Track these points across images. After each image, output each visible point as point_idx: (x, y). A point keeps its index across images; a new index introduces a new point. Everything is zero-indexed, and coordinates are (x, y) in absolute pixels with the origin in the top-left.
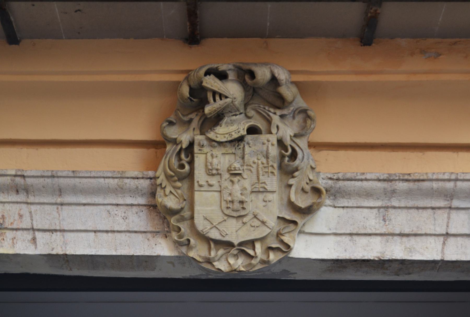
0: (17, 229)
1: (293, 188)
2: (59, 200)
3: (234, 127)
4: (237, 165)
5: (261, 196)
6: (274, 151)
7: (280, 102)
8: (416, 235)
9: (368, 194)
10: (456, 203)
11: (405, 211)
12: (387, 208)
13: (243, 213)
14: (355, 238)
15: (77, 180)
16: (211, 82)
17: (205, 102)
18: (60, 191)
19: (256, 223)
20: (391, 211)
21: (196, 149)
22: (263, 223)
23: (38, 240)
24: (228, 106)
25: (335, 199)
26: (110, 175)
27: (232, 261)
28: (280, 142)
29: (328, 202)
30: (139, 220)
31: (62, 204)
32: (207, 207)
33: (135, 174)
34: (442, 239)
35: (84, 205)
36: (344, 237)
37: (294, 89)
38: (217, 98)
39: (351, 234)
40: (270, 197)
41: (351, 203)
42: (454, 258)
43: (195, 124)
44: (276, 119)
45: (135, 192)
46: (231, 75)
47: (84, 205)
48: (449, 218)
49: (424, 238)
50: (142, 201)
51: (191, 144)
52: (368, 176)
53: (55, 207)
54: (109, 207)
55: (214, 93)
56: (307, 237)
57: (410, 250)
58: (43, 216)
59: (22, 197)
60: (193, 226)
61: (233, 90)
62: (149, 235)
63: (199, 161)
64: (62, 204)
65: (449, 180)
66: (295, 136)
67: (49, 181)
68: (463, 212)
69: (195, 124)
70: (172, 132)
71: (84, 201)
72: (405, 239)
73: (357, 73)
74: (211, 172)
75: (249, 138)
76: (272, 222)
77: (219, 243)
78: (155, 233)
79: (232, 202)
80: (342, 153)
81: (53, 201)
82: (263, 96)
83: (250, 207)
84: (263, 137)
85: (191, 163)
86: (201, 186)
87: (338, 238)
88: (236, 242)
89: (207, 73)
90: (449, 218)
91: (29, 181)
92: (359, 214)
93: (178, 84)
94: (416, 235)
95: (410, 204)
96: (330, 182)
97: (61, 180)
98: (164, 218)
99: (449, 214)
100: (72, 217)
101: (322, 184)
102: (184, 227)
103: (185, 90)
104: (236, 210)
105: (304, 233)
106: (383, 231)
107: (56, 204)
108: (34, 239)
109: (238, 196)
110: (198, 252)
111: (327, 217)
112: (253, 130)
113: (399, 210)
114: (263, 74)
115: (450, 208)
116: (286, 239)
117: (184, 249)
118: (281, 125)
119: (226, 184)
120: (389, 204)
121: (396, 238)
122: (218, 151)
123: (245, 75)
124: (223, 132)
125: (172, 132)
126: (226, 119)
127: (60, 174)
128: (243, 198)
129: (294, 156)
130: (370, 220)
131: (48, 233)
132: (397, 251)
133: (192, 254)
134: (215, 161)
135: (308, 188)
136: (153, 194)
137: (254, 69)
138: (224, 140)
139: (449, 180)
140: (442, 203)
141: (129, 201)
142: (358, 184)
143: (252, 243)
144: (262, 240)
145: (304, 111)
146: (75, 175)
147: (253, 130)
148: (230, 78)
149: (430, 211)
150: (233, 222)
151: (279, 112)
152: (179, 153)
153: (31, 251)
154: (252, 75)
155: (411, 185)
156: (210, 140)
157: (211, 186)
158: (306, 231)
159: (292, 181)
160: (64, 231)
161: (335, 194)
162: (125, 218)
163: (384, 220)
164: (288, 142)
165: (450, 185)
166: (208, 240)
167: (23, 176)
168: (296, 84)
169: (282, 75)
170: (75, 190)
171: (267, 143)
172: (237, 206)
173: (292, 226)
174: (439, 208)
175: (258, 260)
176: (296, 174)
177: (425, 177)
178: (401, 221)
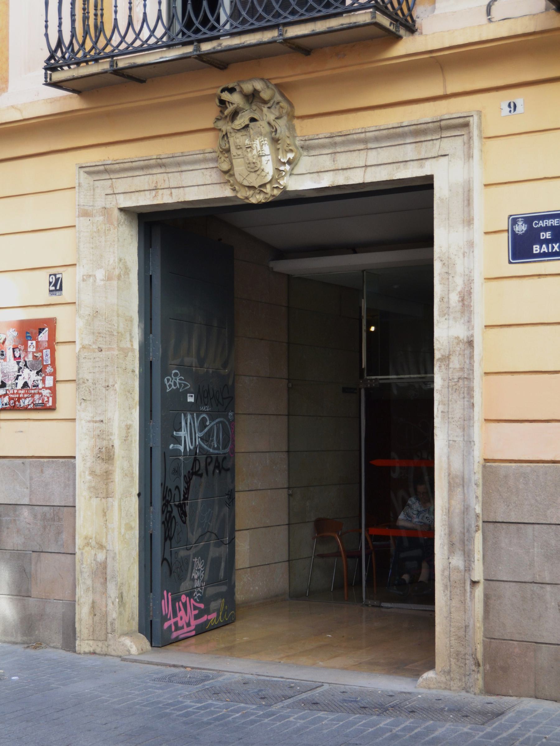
0: (163, 189)
1: (280, 151)
2: (180, 169)
3: (242, 120)
8: (350, 168)
9: (323, 146)
11: (344, 154)
12: (335, 153)
13: (256, 169)
14: (320, 174)
15: (184, 157)
16: (226, 96)
21: (228, 134)
23: (173, 194)
25: (308, 151)
26: (198, 152)
31: (182, 172)
34: (364, 169)
35: (192, 170)
36: (314, 174)
38: (231, 105)
39: (318, 172)
42: (369, 181)
47: (192, 170)
48: (367, 155)
49: (354, 170)
52: (320, 136)
53: (179, 173)
54: (203, 170)
55: (229, 102)
56: (296, 177)
57: (347, 178)
58: (174, 179)
59: (162, 170)
62: (222, 185)
63: (231, 140)
65: (362, 133)
66: (277, 118)
67: (172, 159)
68: (374, 150)
71: (191, 169)
72: (345, 171)
73: (305, 74)
74: (239, 148)
75: (252, 125)
79: (249, 163)
80: (315, 120)
81: (177, 170)
86: (234, 156)
87: (312, 175)
88: (257, 186)
89: (223, 91)
90: (367, 155)
91: (164, 161)
92: (322, 159)
94: (350, 168)
95: (419, 126)
96: (302, 142)
97: (177, 158)
99: (367, 152)
105: (293, 174)
107: (179, 172)
108: (171, 193)
110: (242, 194)
113: (341, 154)
115: (367, 149)
118: (267, 114)
120: (335, 151)
121: (340, 171)
126: (240, 115)
127: (176, 155)
128: (254, 161)
130: (325, 161)
131: (177, 189)
132: (341, 180)
134: (238, 141)
138: (239, 128)
139: (362, 133)
140: (362, 146)
142: (316, 141)
147: (253, 120)
148: (237, 90)
149: (357, 152)
155: (343, 138)
157: (239, 155)
158: (295, 173)
159: (279, 146)
160: (183, 187)
162: (211, 176)
163: (334, 161)
164: (273, 123)
165: (363, 135)
167: (161, 159)
171: (262, 125)
172: (252, 165)
174: (362, 150)
175: (270, 195)
176: (279, 142)
177: (349, 133)
178: (343, 160)
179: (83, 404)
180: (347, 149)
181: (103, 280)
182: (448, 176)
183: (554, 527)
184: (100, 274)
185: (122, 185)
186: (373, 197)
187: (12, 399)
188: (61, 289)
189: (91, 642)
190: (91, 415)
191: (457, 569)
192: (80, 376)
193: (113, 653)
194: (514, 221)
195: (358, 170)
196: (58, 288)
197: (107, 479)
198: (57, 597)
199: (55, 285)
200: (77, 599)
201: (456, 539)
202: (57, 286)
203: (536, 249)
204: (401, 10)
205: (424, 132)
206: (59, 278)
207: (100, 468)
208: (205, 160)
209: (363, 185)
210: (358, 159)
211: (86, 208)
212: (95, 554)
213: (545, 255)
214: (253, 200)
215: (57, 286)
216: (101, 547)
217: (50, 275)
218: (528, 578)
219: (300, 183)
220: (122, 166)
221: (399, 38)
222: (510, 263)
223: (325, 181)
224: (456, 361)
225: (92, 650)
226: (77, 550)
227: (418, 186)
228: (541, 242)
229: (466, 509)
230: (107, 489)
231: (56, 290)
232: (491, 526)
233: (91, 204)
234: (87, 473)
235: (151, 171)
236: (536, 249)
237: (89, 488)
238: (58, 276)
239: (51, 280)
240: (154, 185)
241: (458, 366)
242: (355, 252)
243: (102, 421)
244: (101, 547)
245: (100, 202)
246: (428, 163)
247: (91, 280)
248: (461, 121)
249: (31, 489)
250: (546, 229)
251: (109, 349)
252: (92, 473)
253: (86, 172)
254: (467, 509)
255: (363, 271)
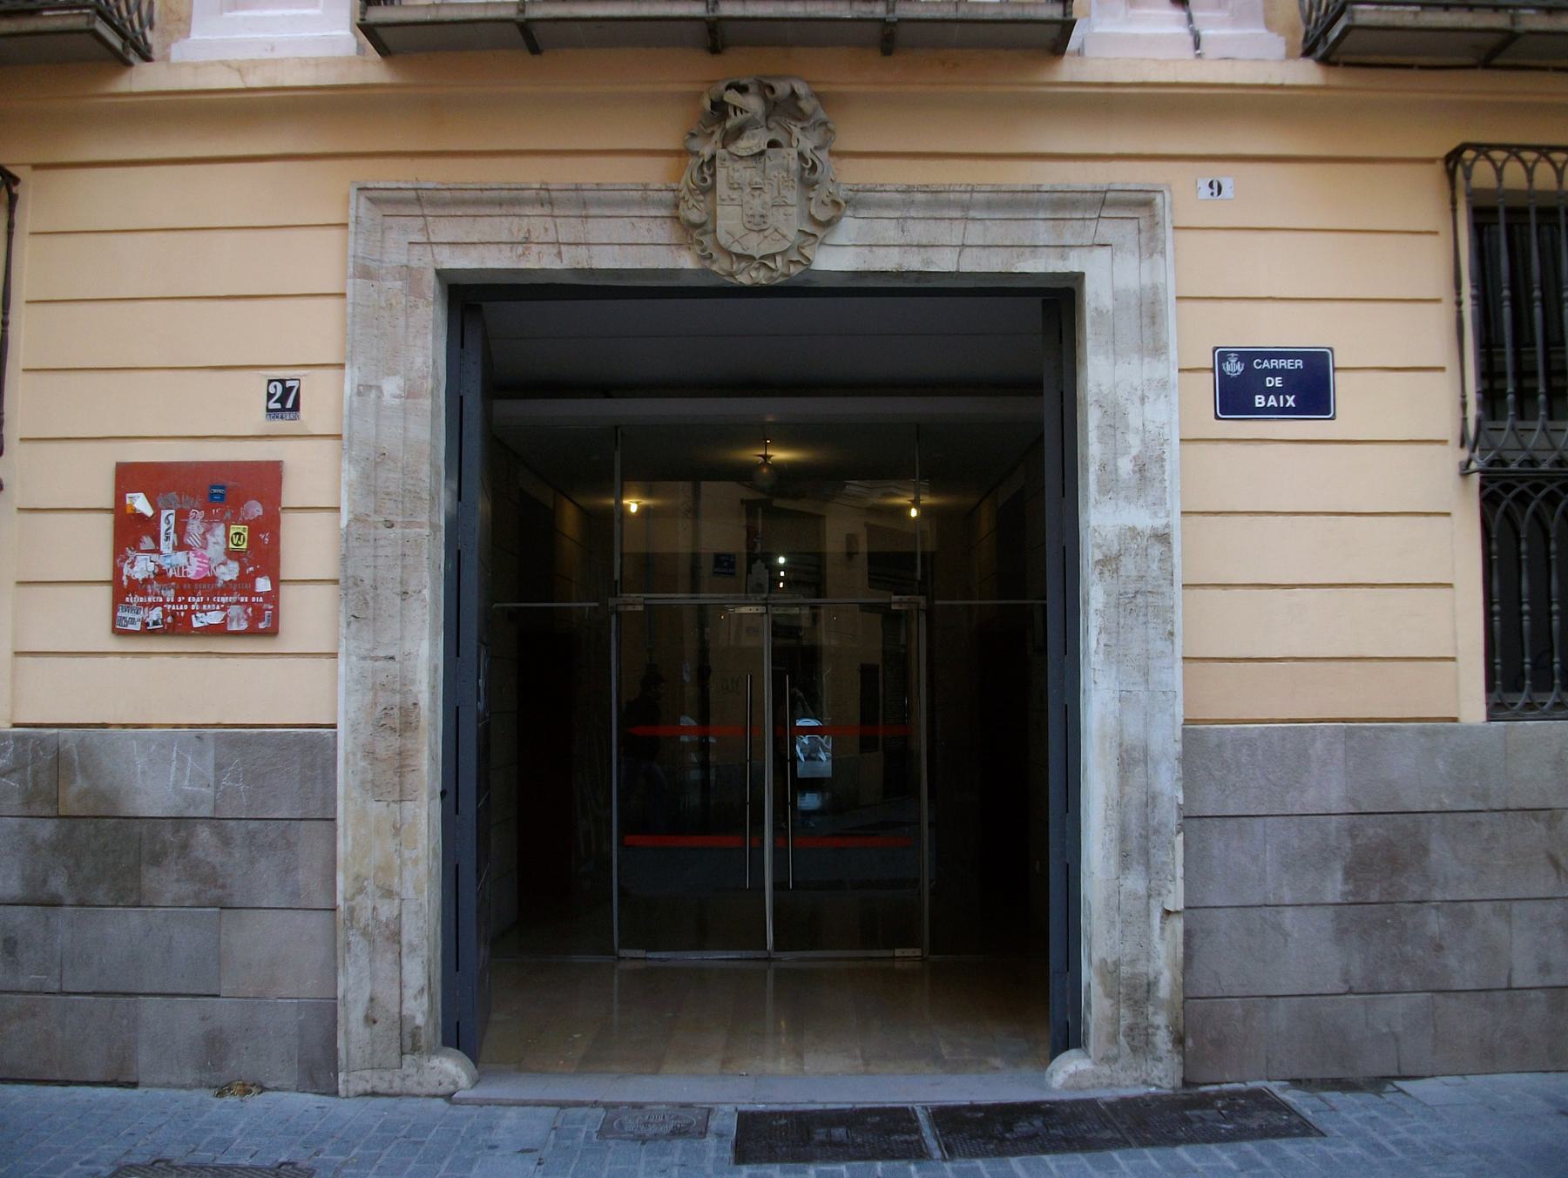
4: (758, 180)
5: (782, 210)
6: (794, 165)
7: (800, 116)
9: (888, 205)
10: (972, 214)
16: (732, 97)
17: (725, 116)
18: (585, 204)
19: (777, 236)
20: (910, 222)
22: (784, 237)
24: (748, 121)
27: (754, 274)
28: (801, 155)
29: (849, 213)
30: (663, 232)
31: (587, 217)
32: (729, 222)
33: (657, 186)
37: (815, 102)
40: (790, 210)
41: (871, 213)
42: (969, 270)
43: (717, 136)
44: (796, 131)
45: (659, 203)
46: (753, 89)
50: (664, 212)
51: (713, 157)
55: (735, 108)
57: (928, 262)
59: (546, 210)
60: (716, 241)
61: (753, 104)
63: (721, 174)
64: (587, 217)
69: (717, 136)
70: (695, 145)
75: (770, 151)
76: (792, 235)
77: (740, 257)
78: (679, 245)
82: (784, 109)
83: (770, 220)
84: (784, 151)
85: (713, 175)
89: (729, 87)
93: (700, 95)
98: (692, 232)
100: (600, 230)
101: (842, 195)
102: (707, 240)
103: (707, 104)
104: (758, 224)
106: (902, 242)
108: (560, 253)
109: (760, 210)
110: (721, 265)
111: (849, 227)
112: (773, 144)
114: (782, 88)
116: (807, 252)
117: (707, 263)
119: (747, 198)
122: (739, 165)
123: (766, 89)
124: (746, 145)
125: (695, 145)
129: (814, 168)
130: (888, 230)
132: (914, 262)
133: (715, 268)
134: (737, 175)
135: (827, 200)
136: (677, 206)
137: (774, 84)
140: (958, 214)
141: (653, 212)
143: (773, 256)
144: (783, 253)
145: (824, 123)
146: (599, 187)
147: (773, 144)
150: (754, 235)
151: (800, 125)
152: (701, 166)
153: (557, 265)
154: (772, 90)
156: (731, 154)
159: (812, 194)
161: (854, 204)
162: (649, 230)
164: (808, 155)
166: (729, 253)
168: (818, 96)
169: (801, 89)
170: (600, 203)
172: (758, 219)
173: (812, 239)
178: (919, 231)
179: (354, 626)
180: (928, 214)
181: (400, 397)
182: (1108, 278)
183: (1296, 819)
184: (391, 386)
185: (445, 230)
186: (869, 299)
187: (173, 614)
188: (296, 407)
189: (367, 1074)
190: (369, 646)
191: (1134, 896)
192: (350, 572)
193: (417, 1090)
194: (1223, 357)
195: (947, 250)
196: (289, 405)
197: (401, 767)
198: (284, 993)
199: (283, 400)
200: (340, 996)
201: (1133, 844)
202: (285, 401)
203: (1259, 401)
204: (131, 22)
205: (1074, 205)
206: (291, 388)
207: (387, 745)
208: (645, 202)
209: (959, 275)
210: (951, 233)
211: (367, 263)
212: (374, 908)
213: (1267, 410)
214: (744, 280)
215: (285, 401)
216: (389, 894)
217: (270, 381)
218: (1257, 900)
219: (837, 258)
220: (458, 194)
221: (129, 64)
222: (1217, 418)
223: (888, 261)
224: (1131, 566)
225: (368, 1088)
226: (340, 901)
227: (1019, 289)
228: (1267, 392)
229: (1150, 800)
230: (401, 784)
231: (283, 409)
232: (1195, 823)
233: (377, 256)
234: (359, 755)
235: (517, 210)
236: (1259, 401)
237: (363, 783)
238: (289, 384)
239: (272, 391)
240: (522, 235)
241: (1134, 573)
242: (608, 396)
243: (392, 658)
244: (389, 894)
245: (396, 254)
246: (1073, 254)
247: (373, 394)
248: (1141, 196)
249: (217, 788)
250: (1274, 373)
251: (408, 525)
252: (370, 754)
253: (369, 199)
254: (1154, 798)
255: (616, 428)
